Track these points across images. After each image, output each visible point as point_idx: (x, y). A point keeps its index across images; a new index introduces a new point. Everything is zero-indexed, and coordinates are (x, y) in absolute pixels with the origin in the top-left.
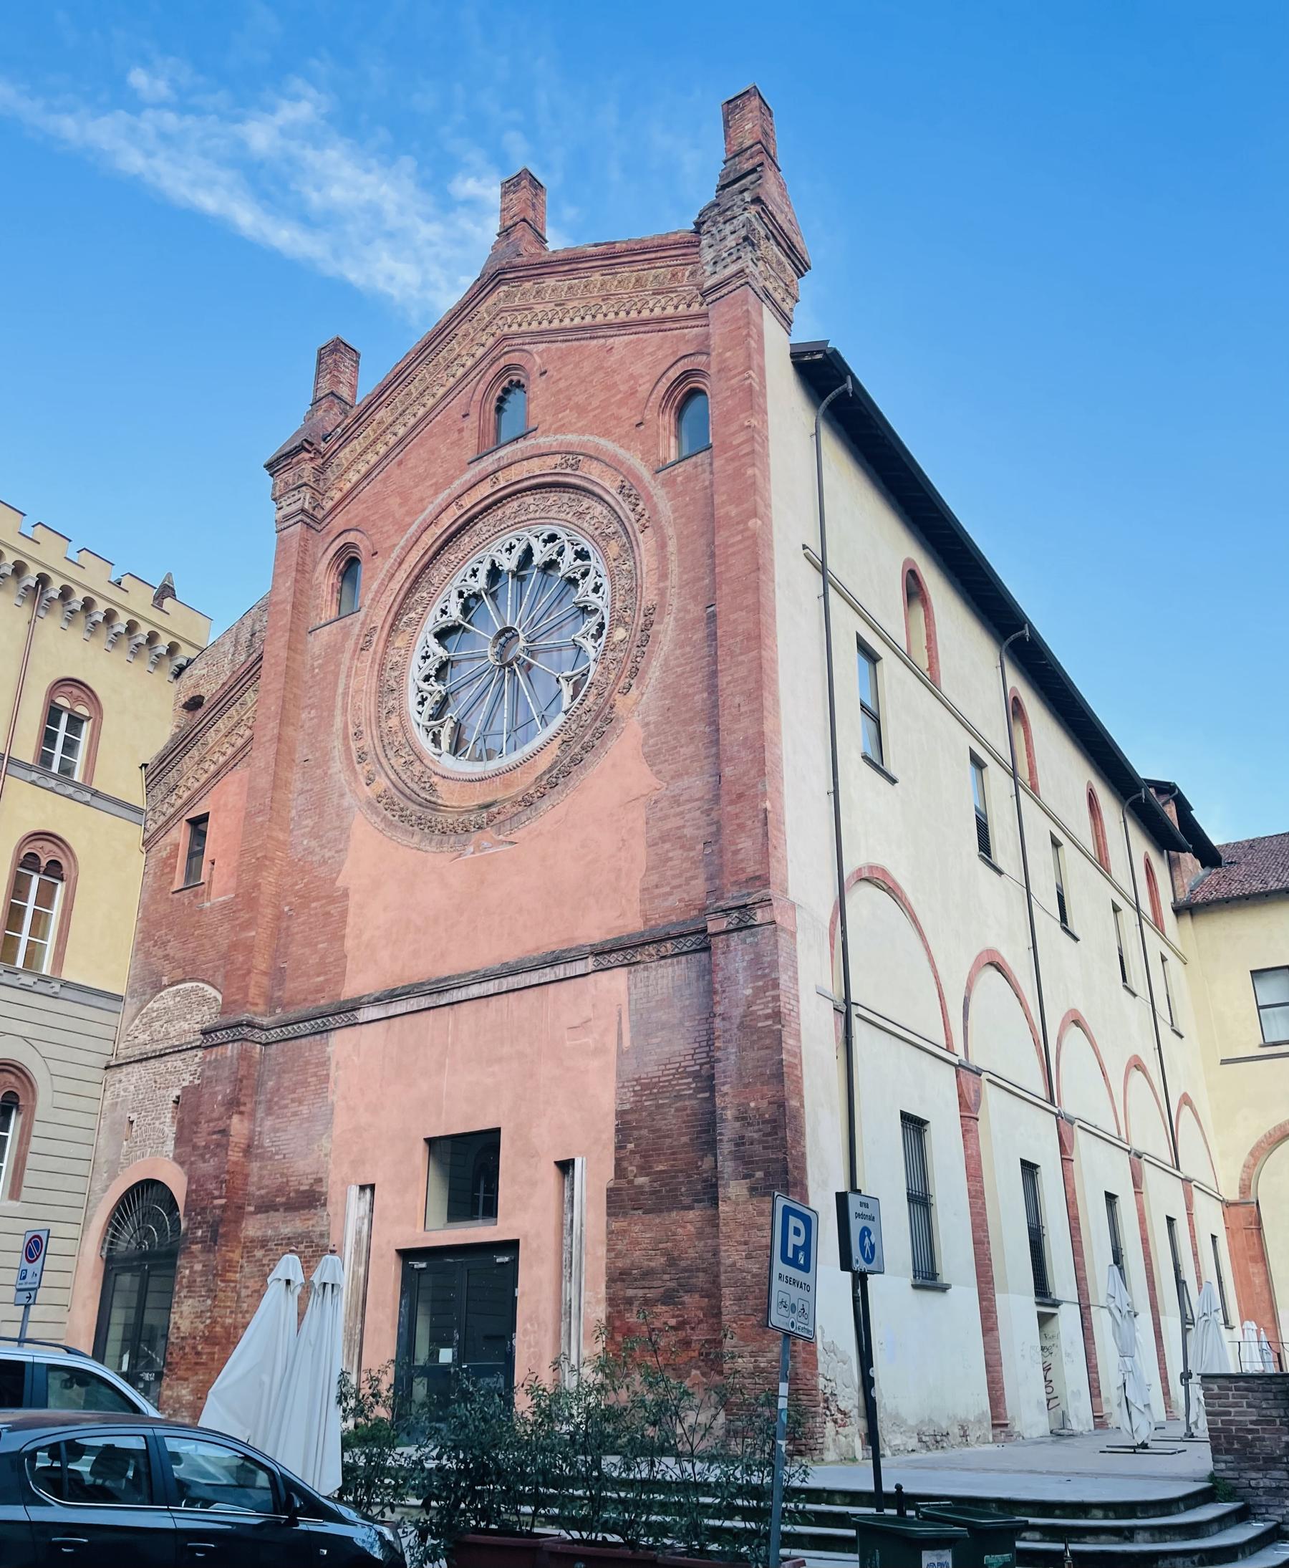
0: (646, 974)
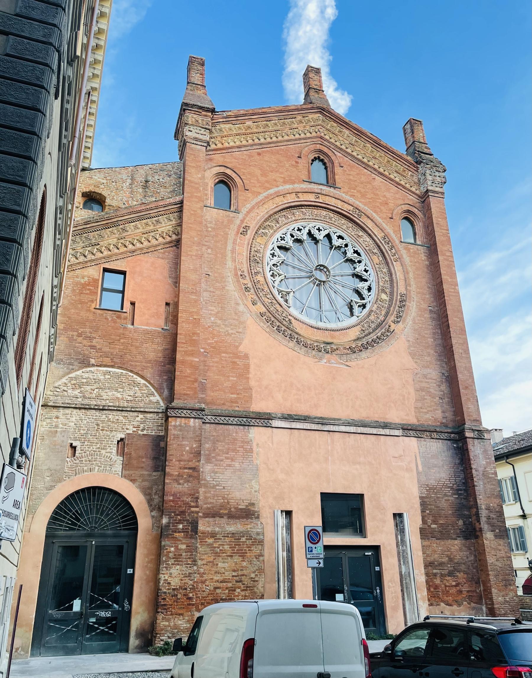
0: (425, 443)
